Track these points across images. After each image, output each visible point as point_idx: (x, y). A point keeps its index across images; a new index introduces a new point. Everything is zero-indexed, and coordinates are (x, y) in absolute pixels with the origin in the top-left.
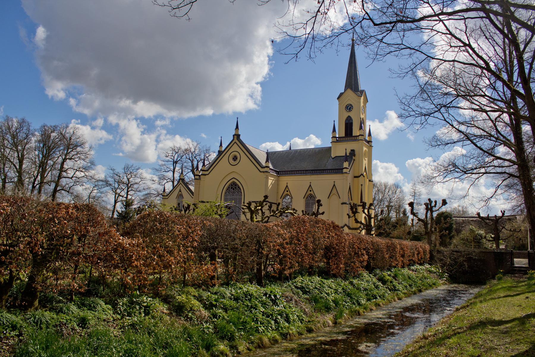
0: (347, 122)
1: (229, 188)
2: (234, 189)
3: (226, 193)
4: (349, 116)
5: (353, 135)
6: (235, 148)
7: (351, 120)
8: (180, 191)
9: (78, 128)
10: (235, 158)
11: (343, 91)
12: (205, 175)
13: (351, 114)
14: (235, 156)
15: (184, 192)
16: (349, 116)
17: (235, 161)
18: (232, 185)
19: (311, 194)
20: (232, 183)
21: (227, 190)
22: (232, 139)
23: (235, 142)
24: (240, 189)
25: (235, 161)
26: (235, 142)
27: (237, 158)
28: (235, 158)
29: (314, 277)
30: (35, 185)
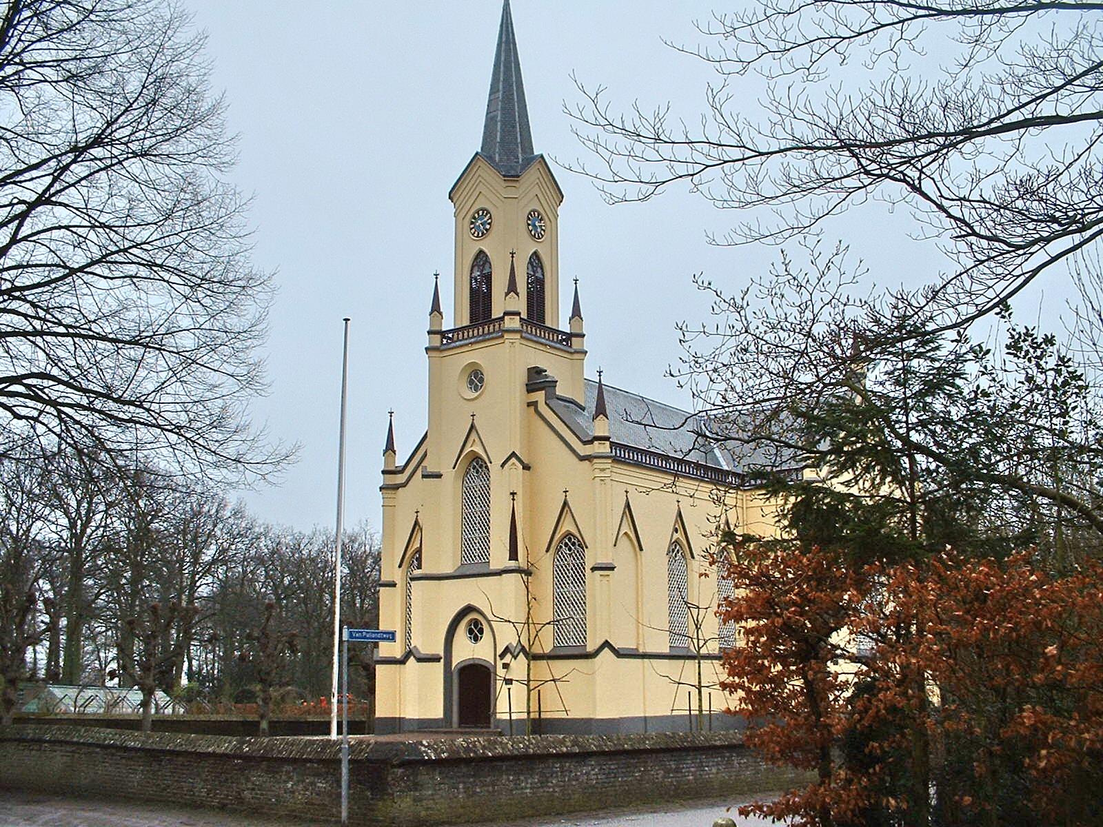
13: (485, 246)
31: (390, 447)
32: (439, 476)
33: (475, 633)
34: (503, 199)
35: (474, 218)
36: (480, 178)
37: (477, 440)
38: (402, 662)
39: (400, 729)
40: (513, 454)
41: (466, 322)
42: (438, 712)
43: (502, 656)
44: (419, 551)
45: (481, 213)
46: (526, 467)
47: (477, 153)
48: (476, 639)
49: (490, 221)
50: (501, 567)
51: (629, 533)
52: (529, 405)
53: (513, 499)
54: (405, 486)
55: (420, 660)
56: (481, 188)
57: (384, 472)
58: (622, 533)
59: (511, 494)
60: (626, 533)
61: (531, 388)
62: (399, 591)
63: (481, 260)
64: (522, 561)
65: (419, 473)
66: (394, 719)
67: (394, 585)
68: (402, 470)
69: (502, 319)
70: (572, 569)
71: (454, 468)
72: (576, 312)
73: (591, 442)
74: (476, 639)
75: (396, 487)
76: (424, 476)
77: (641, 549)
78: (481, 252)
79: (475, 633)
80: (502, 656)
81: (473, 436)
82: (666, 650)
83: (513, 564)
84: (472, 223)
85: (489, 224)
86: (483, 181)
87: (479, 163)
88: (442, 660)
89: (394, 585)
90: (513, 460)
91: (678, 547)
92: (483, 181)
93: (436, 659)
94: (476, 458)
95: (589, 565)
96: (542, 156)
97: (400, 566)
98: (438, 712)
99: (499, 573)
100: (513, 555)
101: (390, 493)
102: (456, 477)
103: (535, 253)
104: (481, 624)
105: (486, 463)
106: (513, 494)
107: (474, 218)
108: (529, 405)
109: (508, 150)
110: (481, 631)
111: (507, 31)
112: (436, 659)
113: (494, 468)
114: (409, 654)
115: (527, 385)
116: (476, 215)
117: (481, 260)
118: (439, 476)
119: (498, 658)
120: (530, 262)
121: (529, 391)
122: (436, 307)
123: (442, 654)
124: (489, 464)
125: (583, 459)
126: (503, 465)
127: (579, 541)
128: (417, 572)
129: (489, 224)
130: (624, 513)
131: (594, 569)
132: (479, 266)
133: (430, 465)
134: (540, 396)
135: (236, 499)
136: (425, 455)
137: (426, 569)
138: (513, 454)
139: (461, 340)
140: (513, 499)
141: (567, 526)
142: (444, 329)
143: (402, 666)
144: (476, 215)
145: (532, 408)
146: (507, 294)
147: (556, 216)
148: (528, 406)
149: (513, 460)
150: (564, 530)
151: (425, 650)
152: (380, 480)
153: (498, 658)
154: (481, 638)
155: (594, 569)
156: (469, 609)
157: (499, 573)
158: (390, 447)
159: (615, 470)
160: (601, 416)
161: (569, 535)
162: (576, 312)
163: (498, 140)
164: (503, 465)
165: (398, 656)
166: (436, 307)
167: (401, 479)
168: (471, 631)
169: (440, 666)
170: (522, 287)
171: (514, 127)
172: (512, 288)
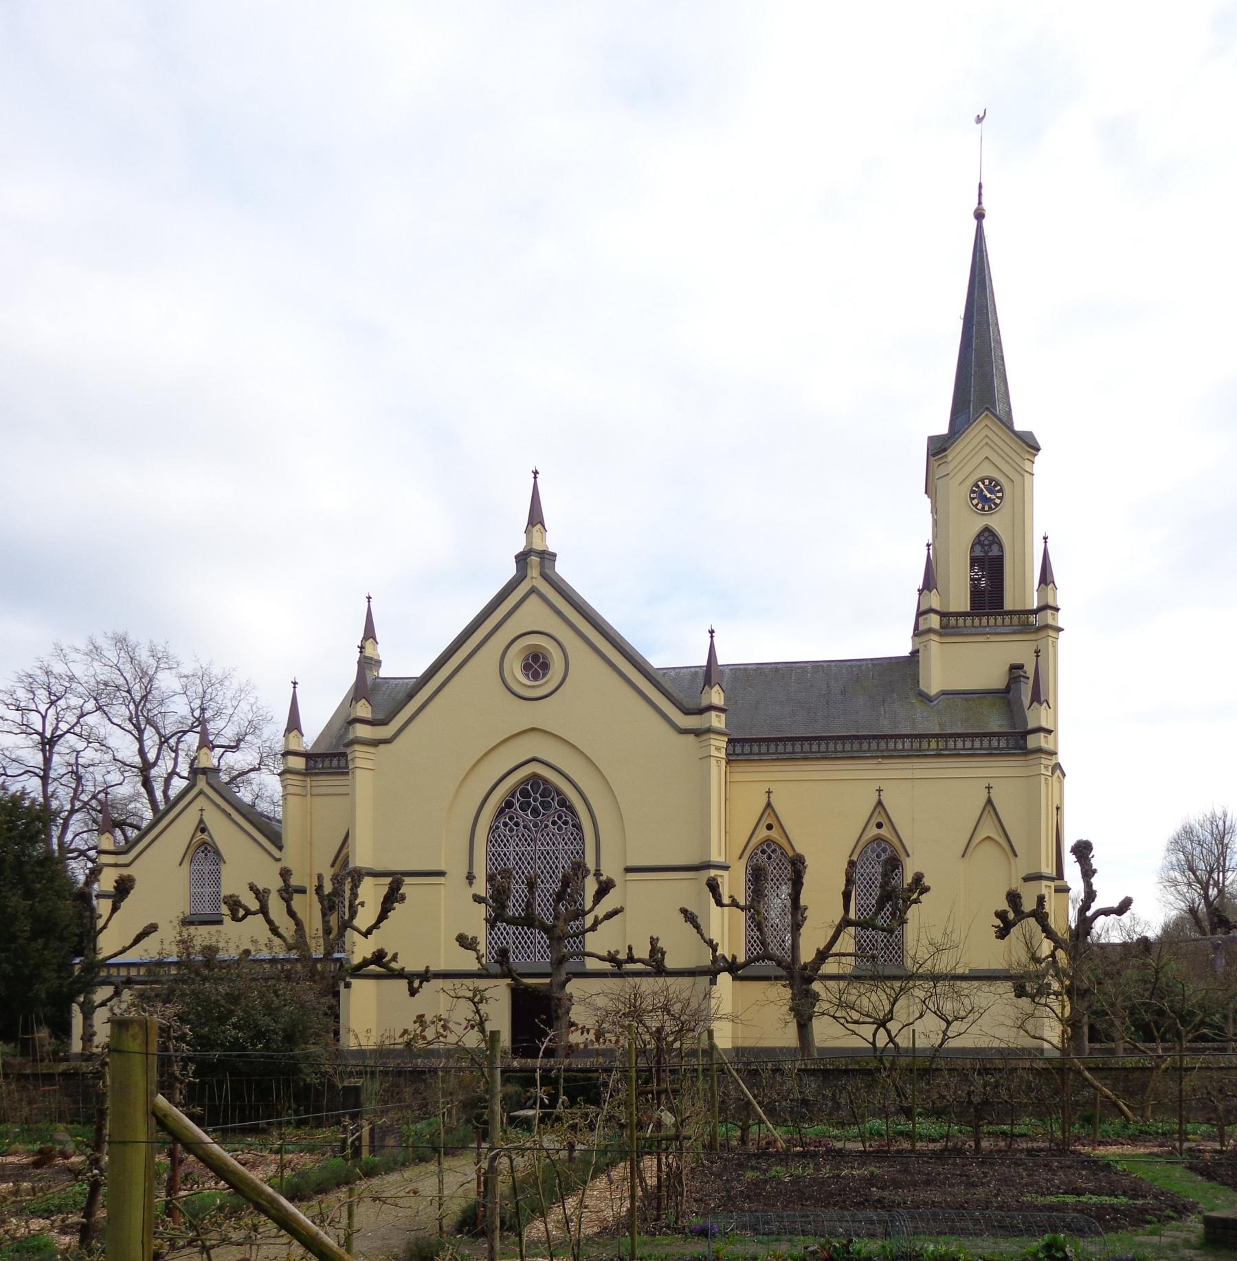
0: (978, 552)
1: (509, 804)
2: (535, 812)
3: (493, 829)
4: (987, 529)
5: (1008, 606)
6: (534, 615)
7: (995, 548)
8: (203, 830)
9: (501, 1195)
10: (536, 664)
11: (944, 430)
12: (387, 741)
13: (996, 522)
14: (536, 657)
15: (224, 833)
16: (987, 529)
17: (536, 677)
18: (525, 794)
19: (204, 843)
20: (525, 781)
21: (501, 812)
22: (511, 571)
23: (533, 590)
24: (571, 810)
25: (536, 677)
26: (533, 590)
27: (545, 667)
28: (536, 664)
29: (78, 870)
30: (1089, 914)
86: (989, 442)
92: (989, 442)
132: (983, 545)
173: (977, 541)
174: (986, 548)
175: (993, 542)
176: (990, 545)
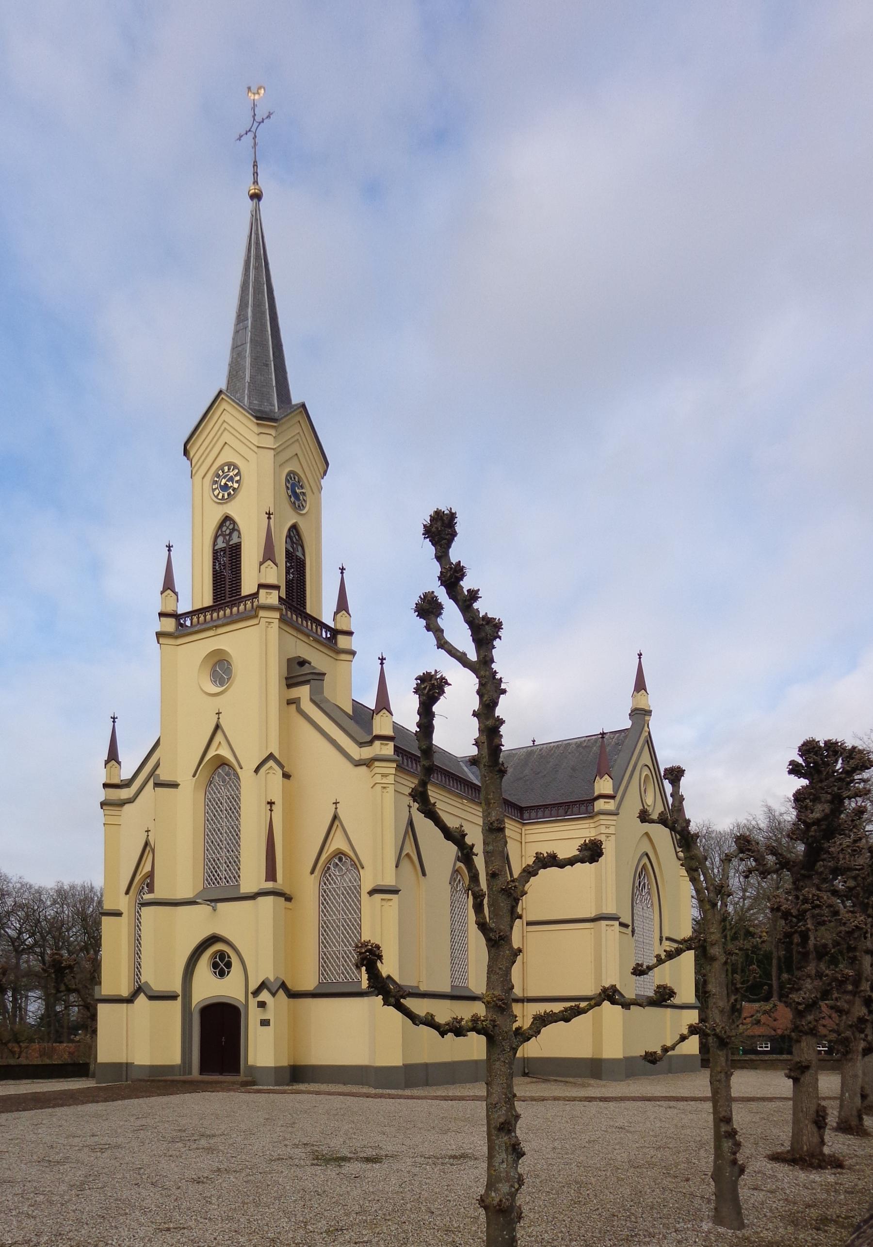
7: (235, 534)
13: (232, 509)
31: (113, 756)
32: (175, 785)
33: (221, 966)
34: (255, 449)
35: (218, 476)
36: (225, 425)
37: (224, 743)
38: (130, 1000)
39: (127, 1078)
40: (271, 756)
41: (208, 601)
42: (174, 1057)
43: (256, 993)
44: (151, 875)
45: (226, 469)
46: (286, 776)
47: (221, 392)
48: (222, 974)
49: (238, 478)
50: (254, 889)
51: (411, 854)
52: (290, 702)
53: (271, 810)
54: (133, 802)
55: (152, 998)
56: (226, 437)
57: (105, 786)
58: (404, 853)
59: (268, 803)
60: (408, 855)
61: (291, 682)
62: (124, 920)
63: (227, 526)
64: (280, 882)
65: (151, 783)
66: (121, 1064)
67: (119, 914)
68: (127, 784)
69: (255, 595)
70: (343, 894)
71: (194, 776)
72: (342, 605)
73: (370, 743)
74: (222, 974)
75: (122, 803)
76: (157, 785)
77: (424, 874)
78: (227, 518)
79: (221, 966)
80: (256, 993)
81: (219, 737)
82: (446, 989)
83: (270, 885)
84: (216, 482)
85: (237, 482)
86: (228, 428)
87: (224, 405)
88: (180, 999)
89: (119, 914)
90: (271, 763)
91: (459, 876)
92: (228, 428)
93: (173, 997)
94: (221, 763)
95: (180, 999)
96: (303, 406)
97: (127, 893)
98: (174, 1057)
99: (253, 897)
100: (271, 875)
101: (112, 811)
102: (196, 788)
103: (294, 528)
104: (229, 957)
105: (234, 770)
106: (271, 803)
107: (218, 476)
108: (290, 702)
109: (258, 389)
110: (229, 965)
111: (257, 234)
112: (173, 997)
113: (246, 775)
114: (138, 990)
115: (286, 679)
116: (220, 472)
117: (227, 526)
118: (175, 785)
119: (250, 996)
120: (289, 536)
121: (289, 686)
122: (169, 585)
123: (179, 991)
124: (239, 770)
125: (358, 764)
126: (257, 771)
127: (352, 860)
128: (148, 897)
129: (237, 482)
130: (406, 832)
131: (371, 893)
132: (224, 536)
133: (164, 775)
134: (303, 692)
135: (498, 1200)
136: (157, 766)
137: (160, 893)
138: (271, 756)
139: (202, 624)
140: (271, 810)
141: (338, 843)
142: (179, 612)
143: (130, 1005)
144: (220, 472)
145: (294, 706)
146: (261, 564)
147: (320, 489)
148: (288, 704)
149: (271, 763)
150: (332, 849)
151: (158, 986)
152: (102, 795)
153: (250, 996)
154: (229, 972)
155: (371, 893)
156: (214, 939)
157: (253, 897)
158: (113, 756)
159: (399, 779)
160: (384, 711)
161: (340, 855)
162: (342, 605)
163: (248, 379)
164: (257, 771)
165: (125, 993)
166: (169, 585)
167: (125, 793)
168: (215, 965)
169: (176, 1006)
170: (281, 555)
171: (267, 365)
172: (268, 555)
173: (220, 532)
174: (227, 538)
175: (234, 530)
176: (230, 534)
